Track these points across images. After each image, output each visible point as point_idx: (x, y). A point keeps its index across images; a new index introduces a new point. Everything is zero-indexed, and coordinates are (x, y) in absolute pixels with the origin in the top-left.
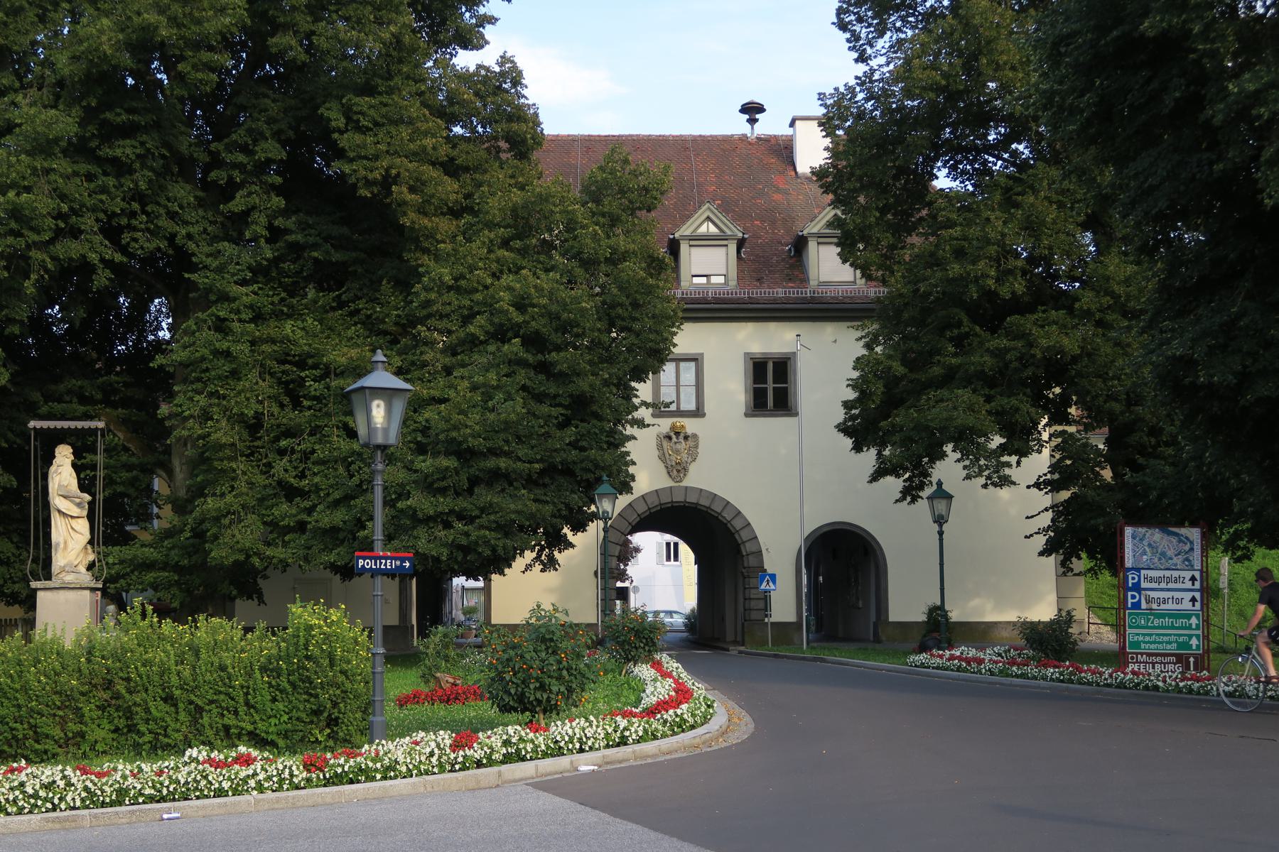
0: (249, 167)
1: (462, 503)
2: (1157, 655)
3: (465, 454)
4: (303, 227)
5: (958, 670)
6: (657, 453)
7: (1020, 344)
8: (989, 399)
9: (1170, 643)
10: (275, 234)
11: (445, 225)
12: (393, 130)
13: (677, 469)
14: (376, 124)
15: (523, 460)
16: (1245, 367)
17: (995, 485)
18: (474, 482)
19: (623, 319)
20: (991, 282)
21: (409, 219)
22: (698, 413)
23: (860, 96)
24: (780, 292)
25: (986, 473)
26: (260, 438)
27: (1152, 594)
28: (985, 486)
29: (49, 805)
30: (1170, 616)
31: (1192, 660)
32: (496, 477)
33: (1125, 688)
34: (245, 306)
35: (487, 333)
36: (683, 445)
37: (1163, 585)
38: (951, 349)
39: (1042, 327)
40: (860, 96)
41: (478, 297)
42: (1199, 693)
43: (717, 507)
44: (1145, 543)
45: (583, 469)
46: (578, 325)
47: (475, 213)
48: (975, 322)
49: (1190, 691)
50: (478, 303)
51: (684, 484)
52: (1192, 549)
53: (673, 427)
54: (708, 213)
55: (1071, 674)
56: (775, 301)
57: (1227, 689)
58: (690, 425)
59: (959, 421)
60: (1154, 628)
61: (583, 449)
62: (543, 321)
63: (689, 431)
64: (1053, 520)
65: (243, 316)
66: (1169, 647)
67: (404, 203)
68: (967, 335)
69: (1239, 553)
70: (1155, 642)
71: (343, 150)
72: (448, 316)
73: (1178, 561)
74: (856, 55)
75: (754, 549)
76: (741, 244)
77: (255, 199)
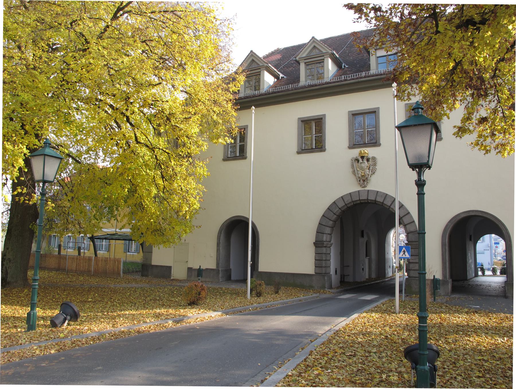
6: (351, 170)
13: (363, 180)
29: (393, 308)
51: (367, 188)
63: (370, 156)
74: (484, 152)
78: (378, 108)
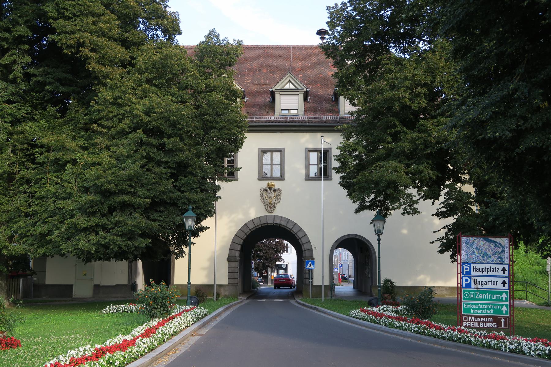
0: (10, 40)
1: (104, 221)
2: (481, 317)
3: (106, 194)
4: (46, 74)
5: (371, 322)
6: (260, 198)
7: (425, 136)
8: (408, 166)
9: (489, 309)
10: (27, 76)
11: (117, 72)
12: (84, 18)
13: (270, 207)
14: (75, 15)
15: (142, 197)
16: (518, 126)
17: (409, 213)
18: (112, 210)
19: (211, 122)
20: (406, 100)
21: (92, 66)
22: (281, 178)
23: (349, 9)
24: (324, 118)
25: (404, 207)
26: (13, 185)
27: (479, 279)
28: (403, 214)
30: (490, 293)
31: (503, 320)
32: (124, 206)
33: (453, 340)
34: (8, 115)
35: (130, 127)
36: (273, 194)
37: (485, 273)
38: (390, 139)
39: (437, 126)
40: (349, 9)
41: (127, 108)
42: (494, 349)
43: (290, 226)
44: (474, 247)
45: (183, 203)
46: (180, 124)
47: (133, 66)
48: (404, 126)
49: (489, 346)
50: (127, 112)
52: (503, 251)
53: (268, 185)
54: (289, 78)
55: (424, 328)
56: (321, 122)
57: (511, 347)
58: (277, 184)
59: (387, 177)
60: (479, 300)
61: (183, 192)
62: (161, 121)
63: (276, 187)
64: (446, 233)
65: (7, 120)
66: (488, 312)
67: (87, 58)
68: (399, 132)
69: (545, 253)
70: (479, 309)
71: (54, 29)
72: (111, 119)
73: (495, 258)
75: (308, 248)
76: (306, 95)
77: (15, 57)
78: (284, 149)
